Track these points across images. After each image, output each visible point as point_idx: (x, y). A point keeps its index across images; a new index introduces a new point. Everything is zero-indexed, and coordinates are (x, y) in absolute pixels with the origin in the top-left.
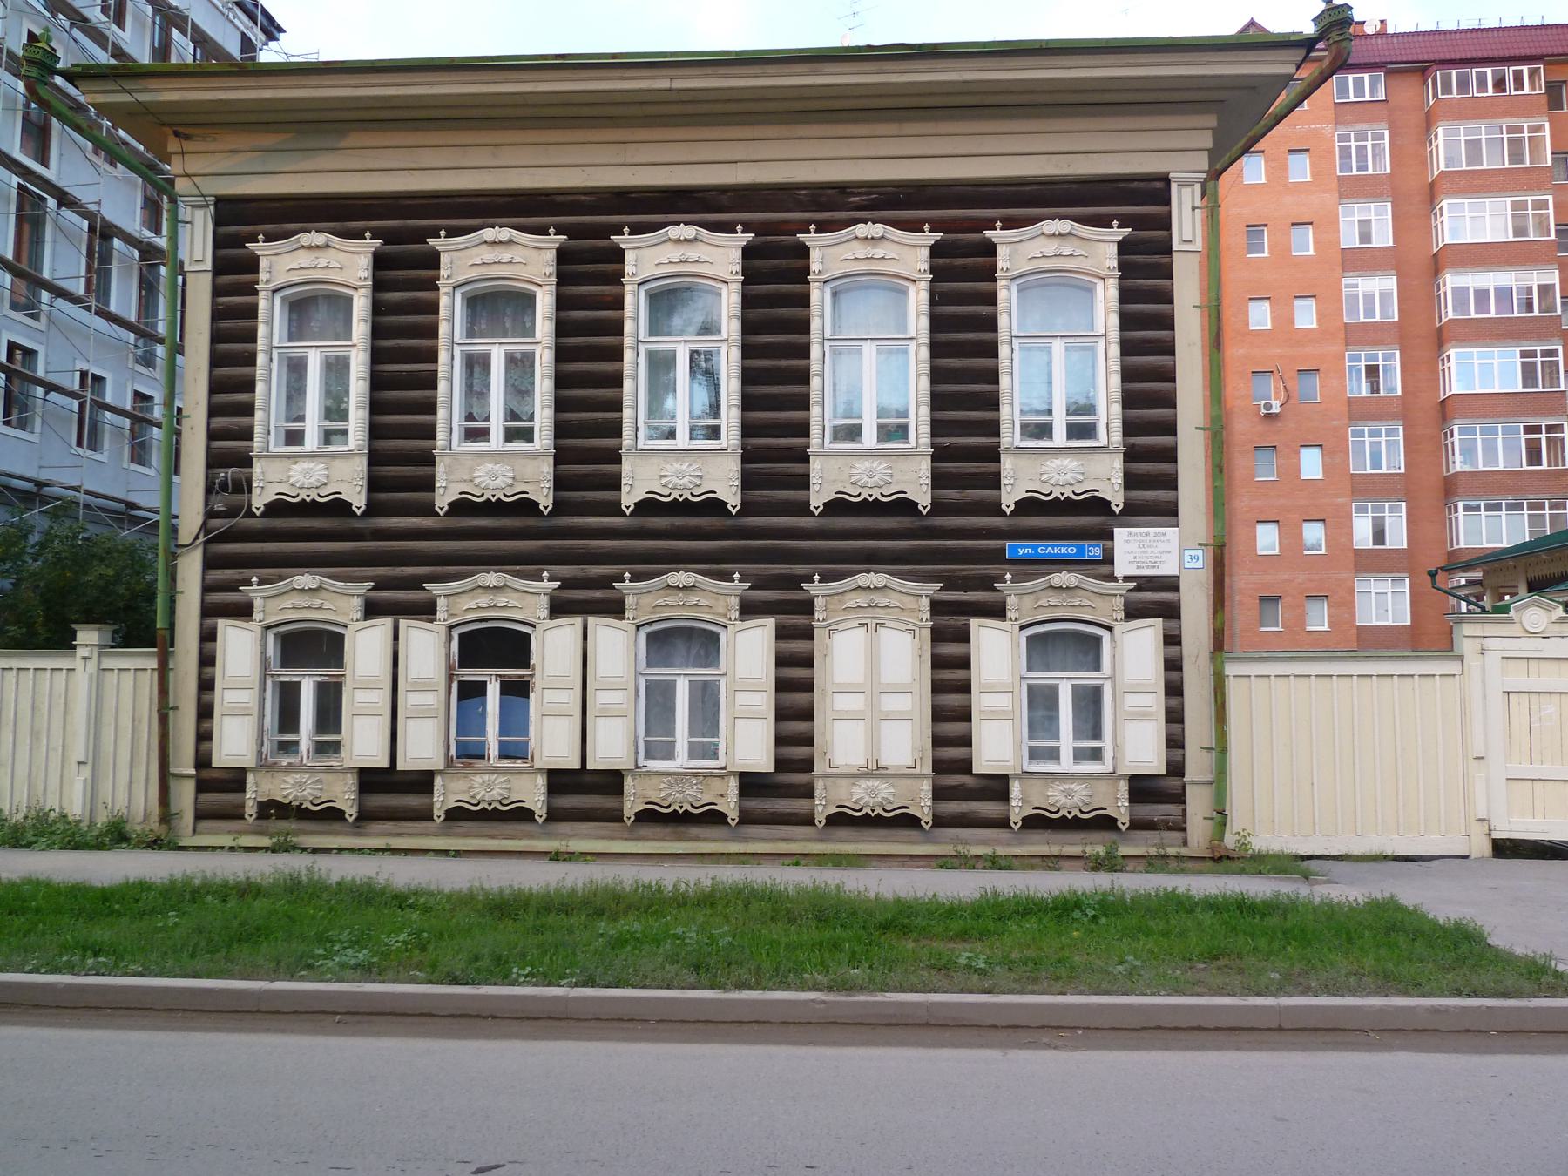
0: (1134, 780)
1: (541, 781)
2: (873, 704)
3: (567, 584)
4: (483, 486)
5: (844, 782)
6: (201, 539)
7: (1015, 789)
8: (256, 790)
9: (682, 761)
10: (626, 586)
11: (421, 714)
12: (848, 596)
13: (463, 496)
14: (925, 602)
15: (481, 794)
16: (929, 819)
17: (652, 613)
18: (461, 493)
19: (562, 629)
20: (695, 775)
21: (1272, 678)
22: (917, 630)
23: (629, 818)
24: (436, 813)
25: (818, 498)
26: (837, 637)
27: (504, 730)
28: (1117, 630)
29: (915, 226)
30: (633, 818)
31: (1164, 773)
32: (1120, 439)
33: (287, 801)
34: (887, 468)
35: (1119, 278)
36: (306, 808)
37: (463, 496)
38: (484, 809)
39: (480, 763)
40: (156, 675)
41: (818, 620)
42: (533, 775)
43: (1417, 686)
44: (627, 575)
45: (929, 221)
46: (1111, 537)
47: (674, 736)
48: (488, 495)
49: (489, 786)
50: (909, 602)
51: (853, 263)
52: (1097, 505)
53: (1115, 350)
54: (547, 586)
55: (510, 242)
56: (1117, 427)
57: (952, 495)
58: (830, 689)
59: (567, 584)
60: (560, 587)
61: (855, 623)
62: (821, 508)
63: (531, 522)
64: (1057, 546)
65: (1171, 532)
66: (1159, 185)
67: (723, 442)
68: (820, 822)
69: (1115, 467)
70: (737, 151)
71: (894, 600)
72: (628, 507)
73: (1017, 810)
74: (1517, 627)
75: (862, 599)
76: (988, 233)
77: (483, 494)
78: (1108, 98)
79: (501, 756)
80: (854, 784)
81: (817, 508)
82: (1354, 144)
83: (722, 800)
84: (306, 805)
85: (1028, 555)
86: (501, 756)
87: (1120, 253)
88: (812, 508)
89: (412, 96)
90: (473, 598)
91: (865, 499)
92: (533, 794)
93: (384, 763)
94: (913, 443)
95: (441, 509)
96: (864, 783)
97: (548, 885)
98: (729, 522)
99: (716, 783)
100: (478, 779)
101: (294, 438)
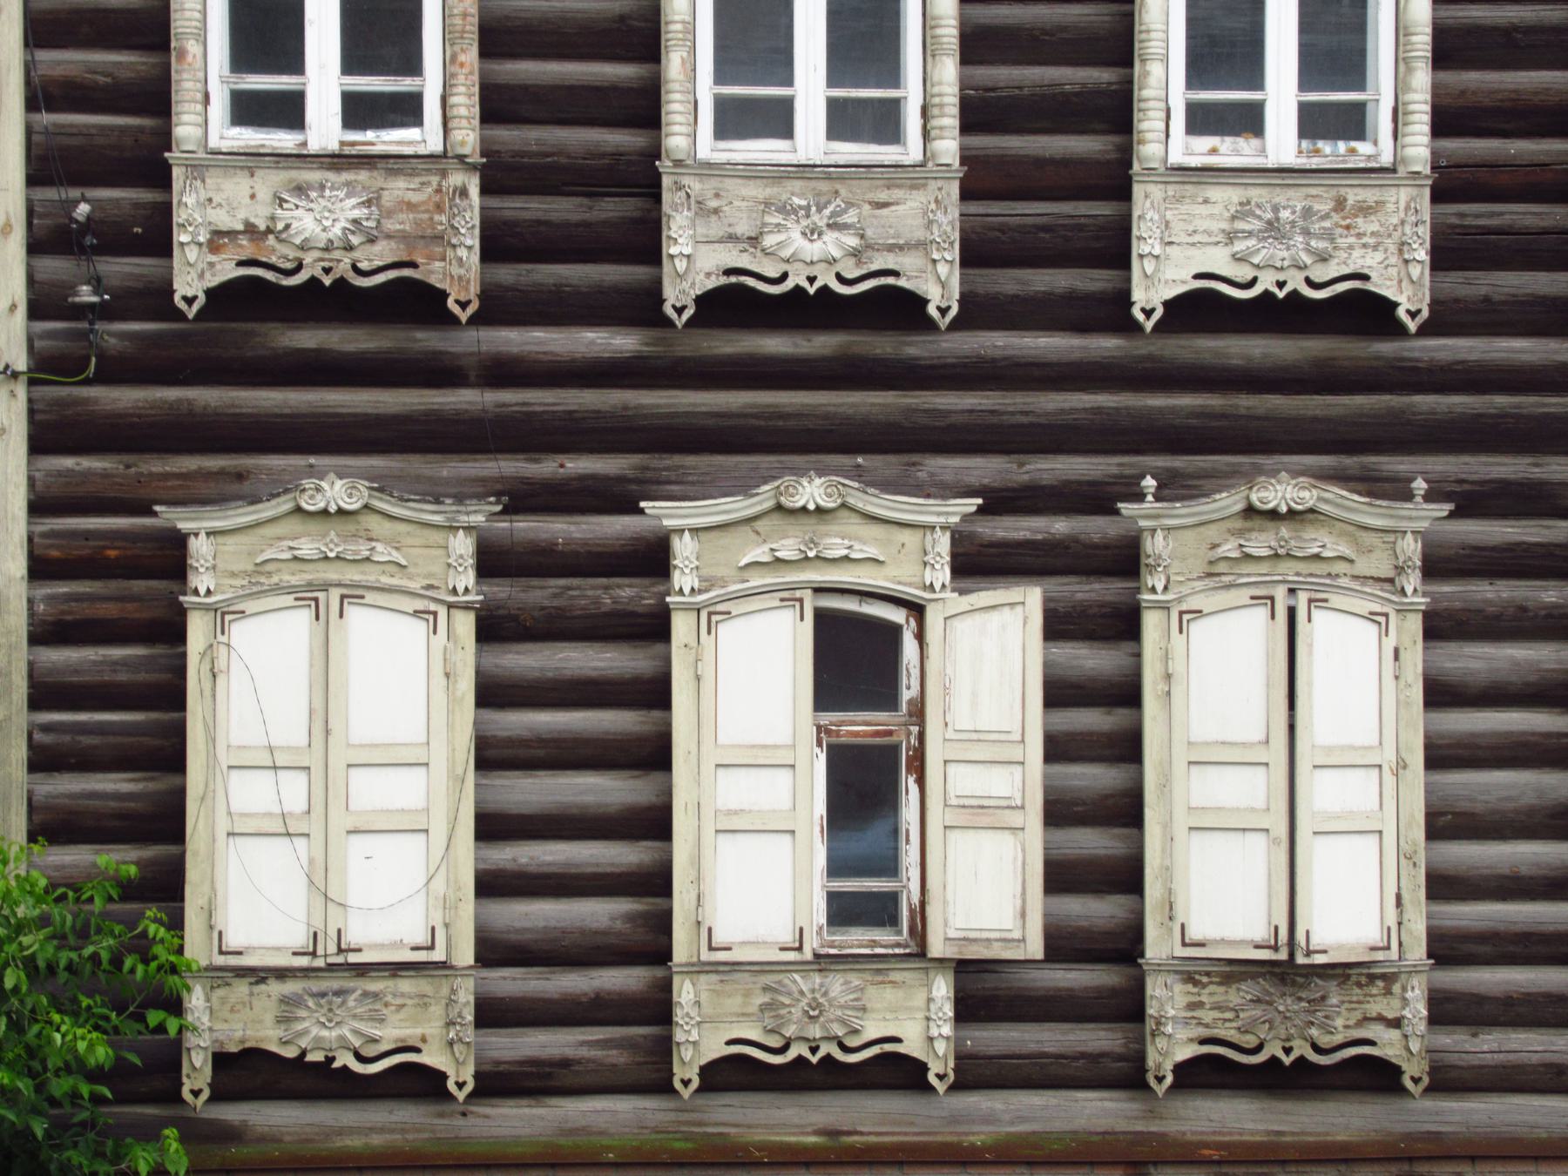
0: (965, 970)
1: (943, 988)
2: (324, 795)
3: (997, 502)
4: (786, 253)
13: (733, 279)
19: (995, 618)
22: (442, 612)
23: (1160, 1079)
24: (679, 1073)
28: (933, 617)
30: (1169, 1080)
31: (1040, 955)
33: (290, 1053)
36: (345, 1068)
37: (733, 279)
38: (800, 1060)
41: (681, 592)
44: (1149, 483)
48: (796, 279)
56: (466, 103)
57: (1008, 281)
60: (981, 510)
63: (1106, 345)
67: (1379, 147)
68: (196, 1093)
72: (1148, 313)
77: (784, 276)
81: (680, 311)
84: (345, 1059)
88: (668, 310)
91: (798, 290)
94: (912, 149)
95: (464, 305)
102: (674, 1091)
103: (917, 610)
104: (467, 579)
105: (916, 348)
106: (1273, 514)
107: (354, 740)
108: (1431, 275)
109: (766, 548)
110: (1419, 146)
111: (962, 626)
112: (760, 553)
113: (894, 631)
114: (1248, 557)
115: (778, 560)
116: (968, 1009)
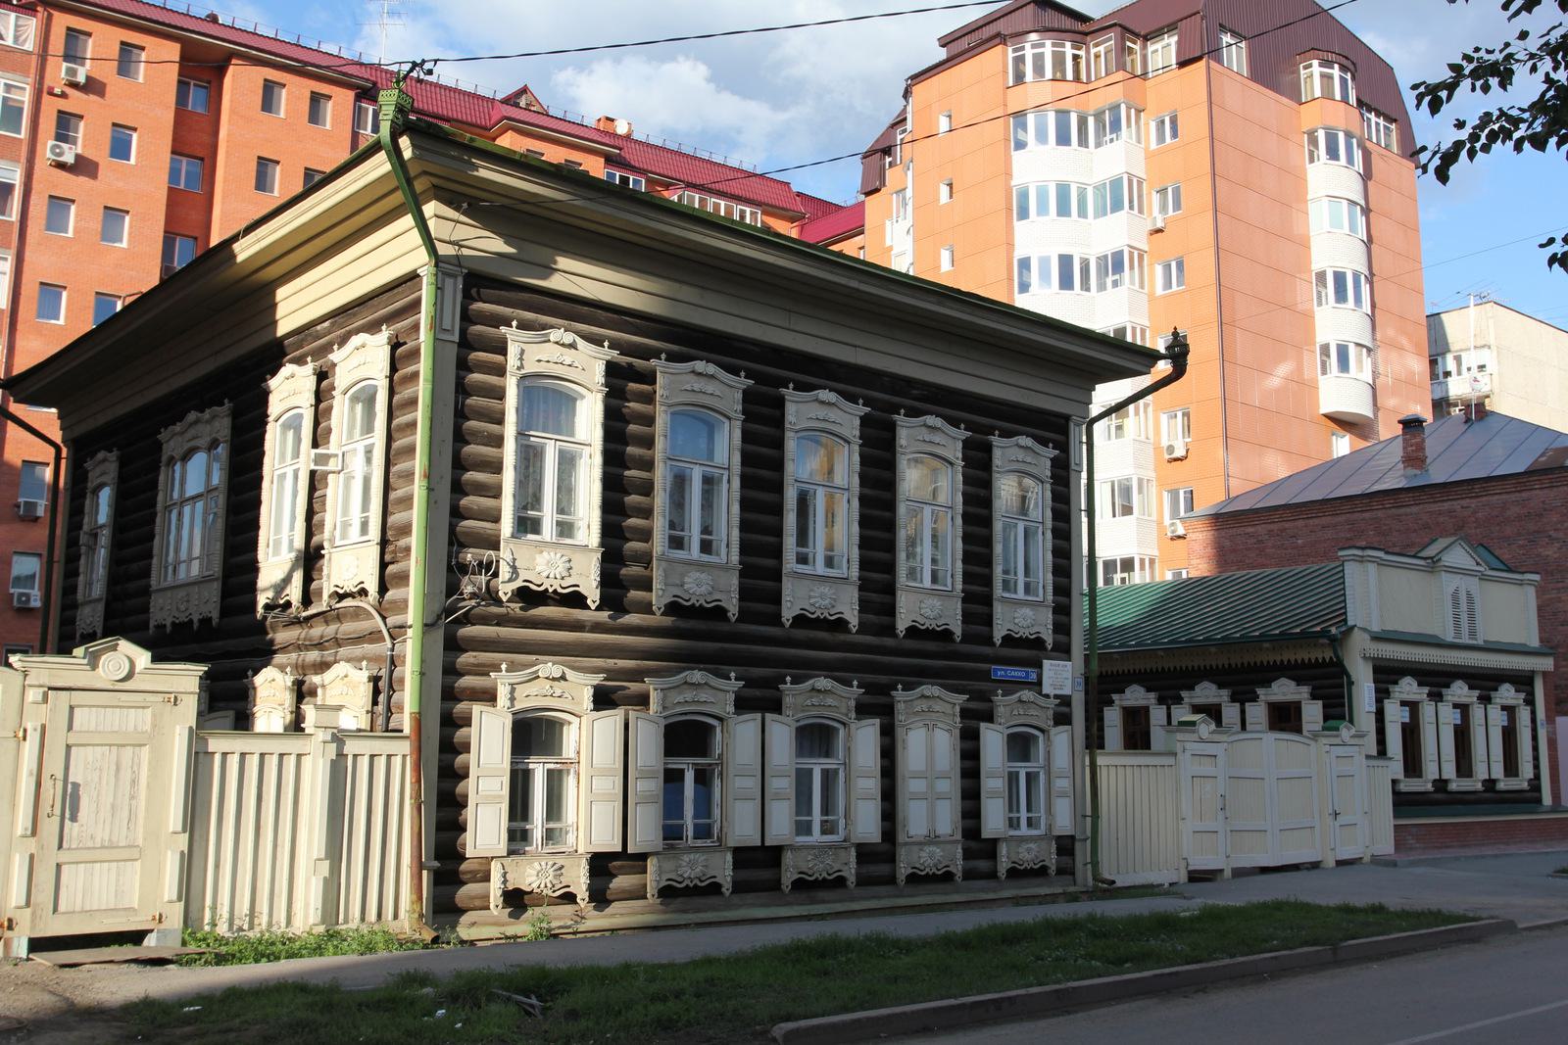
0: (738, 851)
1: (729, 857)
3: (612, 674)
4: (691, 592)
5: (915, 848)
7: (788, 858)
9: (817, 836)
10: (999, 699)
12: (915, 702)
13: (676, 599)
14: (958, 709)
16: (960, 874)
17: (803, 711)
18: (802, 609)
20: (830, 847)
25: (788, 613)
26: (910, 733)
29: (596, 341)
32: (737, 558)
34: (834, 594)
35: (743, 421)
37: (676, 599)
39: (679, 844)
42: (723, 853)
44: (788, 679)
45: (964, 422)
46: (1040, 666)
47: (811, 816)
49: (691, 865)
50: (948, 708)
51: (1016, 463)
52: (1037, 643)
53: (736, 483)
54: (734, 685)
55: (712, 377)
59: (750, 683)
60: (744, 686)
61: (921, 725)
62: (510, 594)
64: (1015, 671)
66: (1063, 421)
70: (968, 367)
71: (938, 706)
73: (1004, 864)
74: (1196, 735)
75: (924, 705)
76: (503, 329)
79: (695, 838)
80: (921, 850)
83: (846, 868)
85: (1002, 676)
86: (695, 838)
87: (862, 424)
89: (1070, 351)
90: (680, 693)
92: (723, 870)
95: (506, 594)
96: (928, 849)
97: (545, 961)
98: (950, 647)
99: (842, 853)
100: (686, 858)
102: (576, 903)
104: (958, 720)
106: (819, 691)
107: (924, 769)
108: (409, 567)
109: (682, 697)
111: (739, 727)
112: (680, 699)
113: (713, 727)
114: (813, 705)
115: (686, 702)
116: (737, 865)
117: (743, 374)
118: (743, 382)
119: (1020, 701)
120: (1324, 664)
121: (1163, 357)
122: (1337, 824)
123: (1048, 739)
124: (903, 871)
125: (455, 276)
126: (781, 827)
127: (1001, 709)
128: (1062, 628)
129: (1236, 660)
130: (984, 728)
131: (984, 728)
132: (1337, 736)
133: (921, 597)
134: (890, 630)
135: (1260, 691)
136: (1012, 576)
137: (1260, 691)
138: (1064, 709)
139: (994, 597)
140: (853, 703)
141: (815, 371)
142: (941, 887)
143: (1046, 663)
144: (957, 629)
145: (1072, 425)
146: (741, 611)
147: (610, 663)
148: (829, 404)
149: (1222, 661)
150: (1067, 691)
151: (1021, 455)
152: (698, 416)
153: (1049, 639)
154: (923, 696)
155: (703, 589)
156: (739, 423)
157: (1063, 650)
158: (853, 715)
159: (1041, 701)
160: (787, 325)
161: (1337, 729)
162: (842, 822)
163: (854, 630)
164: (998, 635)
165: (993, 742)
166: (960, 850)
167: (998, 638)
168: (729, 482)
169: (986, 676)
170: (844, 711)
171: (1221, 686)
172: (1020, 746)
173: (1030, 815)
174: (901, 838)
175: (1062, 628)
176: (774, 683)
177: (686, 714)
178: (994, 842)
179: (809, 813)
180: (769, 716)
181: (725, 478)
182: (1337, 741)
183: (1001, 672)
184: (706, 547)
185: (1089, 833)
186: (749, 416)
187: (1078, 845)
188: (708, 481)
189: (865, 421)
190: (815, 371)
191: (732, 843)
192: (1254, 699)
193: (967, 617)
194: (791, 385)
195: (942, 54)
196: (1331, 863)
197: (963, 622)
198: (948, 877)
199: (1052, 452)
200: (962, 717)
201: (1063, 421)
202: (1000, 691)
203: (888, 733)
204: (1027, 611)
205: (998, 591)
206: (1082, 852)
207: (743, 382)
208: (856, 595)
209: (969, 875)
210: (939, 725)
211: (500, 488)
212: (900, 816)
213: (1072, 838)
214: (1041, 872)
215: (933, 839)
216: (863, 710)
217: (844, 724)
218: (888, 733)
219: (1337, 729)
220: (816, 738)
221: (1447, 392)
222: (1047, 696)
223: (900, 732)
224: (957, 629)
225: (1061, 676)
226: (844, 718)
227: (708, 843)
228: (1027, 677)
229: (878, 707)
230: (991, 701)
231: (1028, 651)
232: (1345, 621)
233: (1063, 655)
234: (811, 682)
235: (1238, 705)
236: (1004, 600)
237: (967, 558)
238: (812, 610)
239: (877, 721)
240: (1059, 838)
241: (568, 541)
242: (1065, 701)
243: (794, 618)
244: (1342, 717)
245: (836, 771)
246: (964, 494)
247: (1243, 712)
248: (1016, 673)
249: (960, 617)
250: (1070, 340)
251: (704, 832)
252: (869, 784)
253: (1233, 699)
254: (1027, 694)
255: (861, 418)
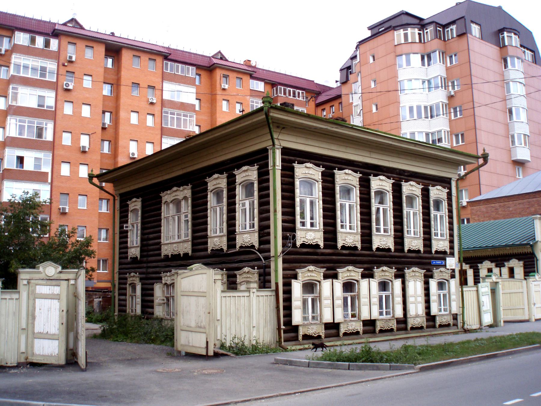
0: (397, 319)
1: (361, 323)
6: (281, 255)
7: (342, 326)
8: (301, 332)
11: (339, 307)
14: (423, 274)
15: (350, 328)
16: (425, 327)
21: (8, 300)
26: (410, 283)
27: (352, 311)
28: (394, 281)
40: (275, 297)
43: (14, 303)
46: (445, 260)
51: (344, 180)
52: (445, 253)
53: (321, 202)
58: (409, 296)
65: (454, 258)
66: (449, 180)
69: (358, 238)
70: (422, 165)
71: (417, 274)
78: (450, 161)
82: (182, 118)
84: (313, 335)
90: (346, 273)
92: (359, 327)
93: (332, 321)
98: (337, 251)
101: (303, 224)
103: (319, 282)
104: (423, 278)
105: (357, 252)
110: (393, 233)
117: (359, 172)
118: (359, 175)
119: (348, 270)
120: (528, 254)
121: (480, 158)
122: (535, 307)
123: (359, 284)
124: (409, 326)
125: (279, 149)
126: (375, 315)
127: (435, 274)
128: (452, 248)
129: (497, 253)
130: (294, 282)
131: (294, 282)
132: (490, 279)
133: (411, 240)
134: (370, 248)
135: (506, 263)
136: (344, 224)
137: (506, 263)
138: (453, 273)
139: (297, 228)
140: (393, 274)
141: (378, 170)
142: (420, 331)
143: (447, 259)
144: (422, 249)
145: (452, 181)
146: (361, 247)
147: (328, 265)
148: (383, 180)
149: (492, 253)
150: (453, 268)
151: (437, 192)
152: (309, 183)
153: (448, 251)
154: (413, 271)
155: (351, 241)
156: (358, 188)
157: (452, 254)
158: (393, 278)
159: (447, 271)
160: (369, 156)
161: (534, 276)
162: (391, 311)
163: (322, 248)
164: (433, 250)
165: (433, 284)
166: (425, 319)
167: (433, 252)
168: (356, 207)
169: (430, 264)
170: (391, 277)
171: (492, 262)
172: (441, 285)
173: (314, 315)
174: (408, 316)
175: (452, 248)
176: (371, 269)
177: (313, 280)
178: (434, 317)
179: (347, 311)
180: (371, 279)
181: (355, 206)
182: (535, 280)
183: (434, 262)
184: (312, 225)
185: (461, 313)
186: (324, 181)
187: (458, 317)
188: (312, 203)
189: (323, 174)
190: (378, 170)
191: (362, 319)
192: (504, 266)
193: (425, 246)
194: (337, 169)
195: (369, 34)
196: (533, 320)
197: (424, 247)
198: (422, 328)
199: (447, 191)
200: (424, 277)
201: (449, 180)
202: (375, 267)
203: (403, 283)
204: (441, 242)
205: (298, 225)
206: (460, 318)
207: (359, 175)
208: (360, 238)
209: (398, 329)
210: (418, 280)
211: (269, 210)
212: (408, 309)
213: (456, 314)
214: (448, 325)
215: (417, 316)
216: (397, 276)
217: (391, 281)
218: (403, 283)
219: (534, 276)
220: (384, 286)
221: (341, 92)
222: (448, 269)
223: (407, 283)
224: (422, 249)
225: (452, 262)
226: (391, 279)
227: (355, 319)
228: (442, 263)
229: (400, 275)
230: (432, 271)
231: (442, 255)
232: (535, 239)
233: (452, 256)
234: (307, 268)
235: (499, 268)
236: (435, 239)
237: (424, 227)
238: (381, 245)
239: (400, 280)
240: (453, 314)
241: (314, 228)
242: (453, 270)
243: (341, 247)
244: (534, 272)
245: (389, 296)
246: (422, 206)
247: (500, 271)
248: (439, 262)
249: (422, 246)
250: (312, 121)
251: (353, 316)
252: (399, 299)
253: (496, 266)
254: (442, 269)
255: (392, 184)
